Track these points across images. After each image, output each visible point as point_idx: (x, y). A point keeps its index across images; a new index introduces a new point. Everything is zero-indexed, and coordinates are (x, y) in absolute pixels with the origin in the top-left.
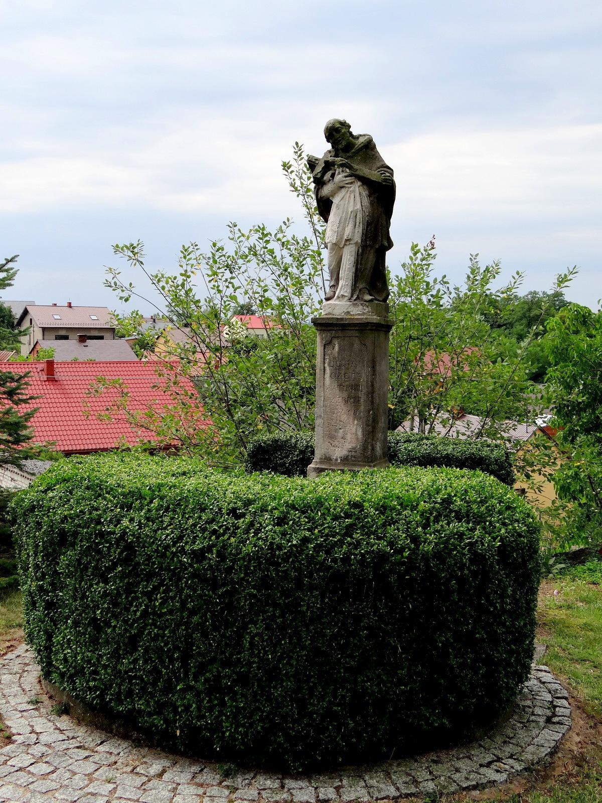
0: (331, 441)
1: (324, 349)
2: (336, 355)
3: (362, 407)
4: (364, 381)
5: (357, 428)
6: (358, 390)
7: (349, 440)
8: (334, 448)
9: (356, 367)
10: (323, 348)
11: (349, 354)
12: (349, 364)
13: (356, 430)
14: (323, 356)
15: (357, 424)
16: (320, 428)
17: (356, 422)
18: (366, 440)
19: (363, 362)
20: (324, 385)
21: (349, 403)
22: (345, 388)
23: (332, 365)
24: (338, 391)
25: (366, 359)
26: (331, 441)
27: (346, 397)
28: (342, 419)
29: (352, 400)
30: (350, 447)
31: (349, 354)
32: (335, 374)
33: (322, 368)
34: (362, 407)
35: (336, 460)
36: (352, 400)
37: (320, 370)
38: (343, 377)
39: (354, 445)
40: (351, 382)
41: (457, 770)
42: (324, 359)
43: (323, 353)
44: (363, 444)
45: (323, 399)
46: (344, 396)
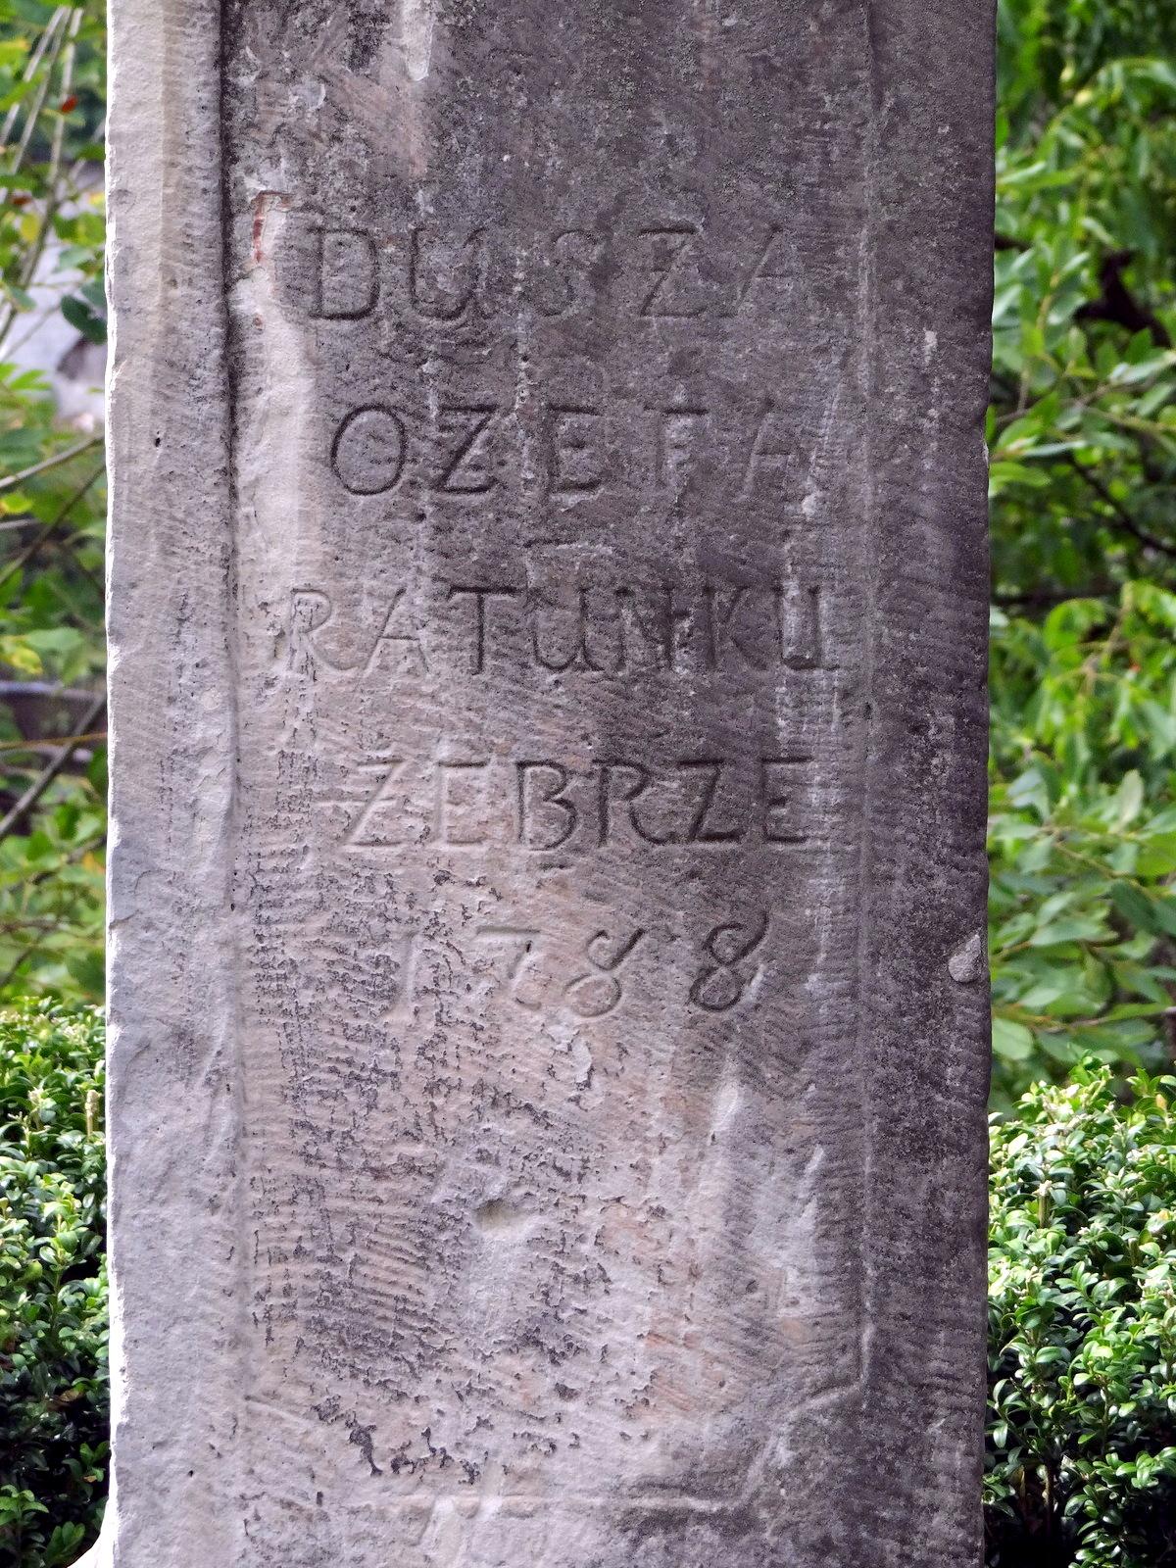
0: (350, 1394)
1: (224, 58)
2: (413, 145)
3: (825, 885)
4: (839, 510)
5: (744, 1188)
6: (755, 649)
7: (635, 1361)
8: (399, 1495)
9: (712, 315)
10: (201, 43)
11: (603, 121)
12: (602, 275)
13: (738, 1216)
14: (202, 159)
15: (755, 1134)
16: (180, 1215)
17: (729, 1103)
18: (885, 1359)
19: (822, 248)
20: (232, 590)
21: (623, 839)
22: (553, 624)
23: (343, 284)
24: (441, 665)
25: (865, 192)
26: (350, 1394)
27: (582, 756)
28: (522, 1073)
29: (670, 791)
30: (646, 1458)
31: (603, 121)
32: (403, 417)
33: (205, 338)
34: (825, 885)
35: (1091, 1189)
36: (670, 791)
37: (173, 368)
38: (523, 467)
39: (709, 1432)
40: (648, 533)
41: (753, 1156)
42: (227, 210)
43: (203, 123)
44: (847, 1412)
45: (216, 798)
46: (546, 737)
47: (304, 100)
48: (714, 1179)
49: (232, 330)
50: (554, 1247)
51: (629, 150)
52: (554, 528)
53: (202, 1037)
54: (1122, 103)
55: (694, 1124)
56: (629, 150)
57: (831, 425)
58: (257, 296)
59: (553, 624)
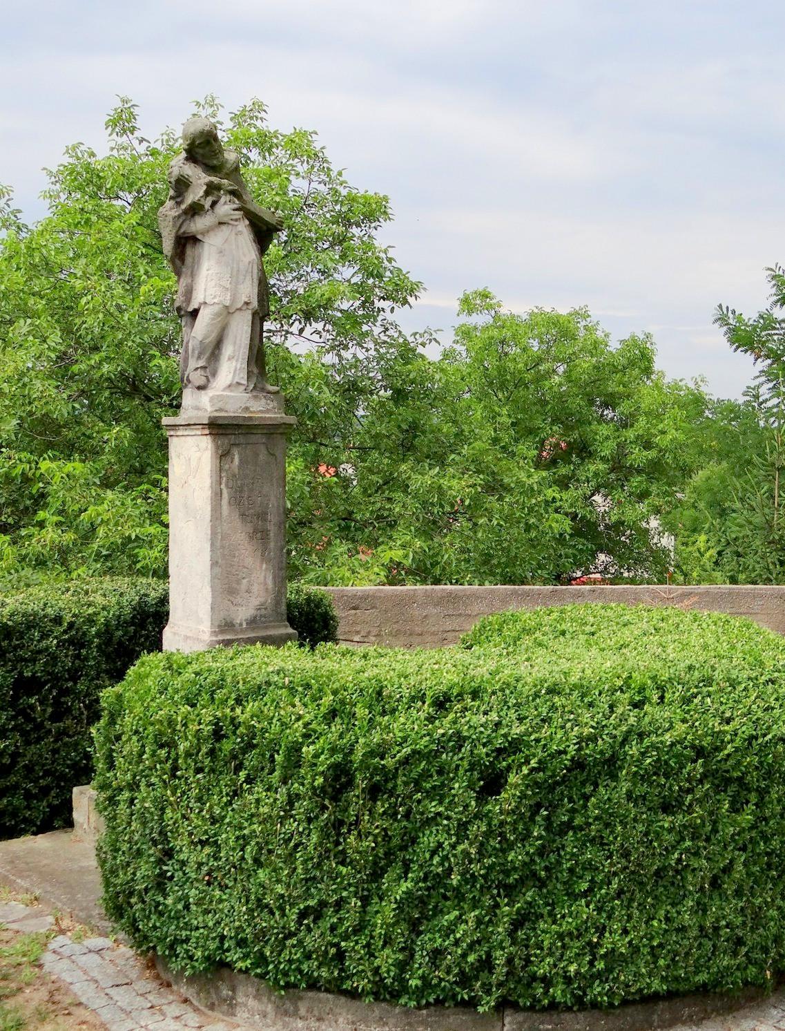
2: (236, 471)
6: (266, 520)
7: (256, 593)
13: (265, 578)
15: (266, 569)
17: (264, 566)
18: (279, 591)
30: (258, 603)
31: (253, 468)
32: (236, 498)
39: (262, 600)
42: (221, 477)
47: (227, 467)
48: (263, 574)
49: (221, 490)
50: (249, 582)
51: (255, 471)
52: (249, 509)
53: (240, 118)
54: (391, 634)
55: (261, 567)
56: (255, 471)
57: (272, 498)
58: (223, 486)
59: (249, 519)
